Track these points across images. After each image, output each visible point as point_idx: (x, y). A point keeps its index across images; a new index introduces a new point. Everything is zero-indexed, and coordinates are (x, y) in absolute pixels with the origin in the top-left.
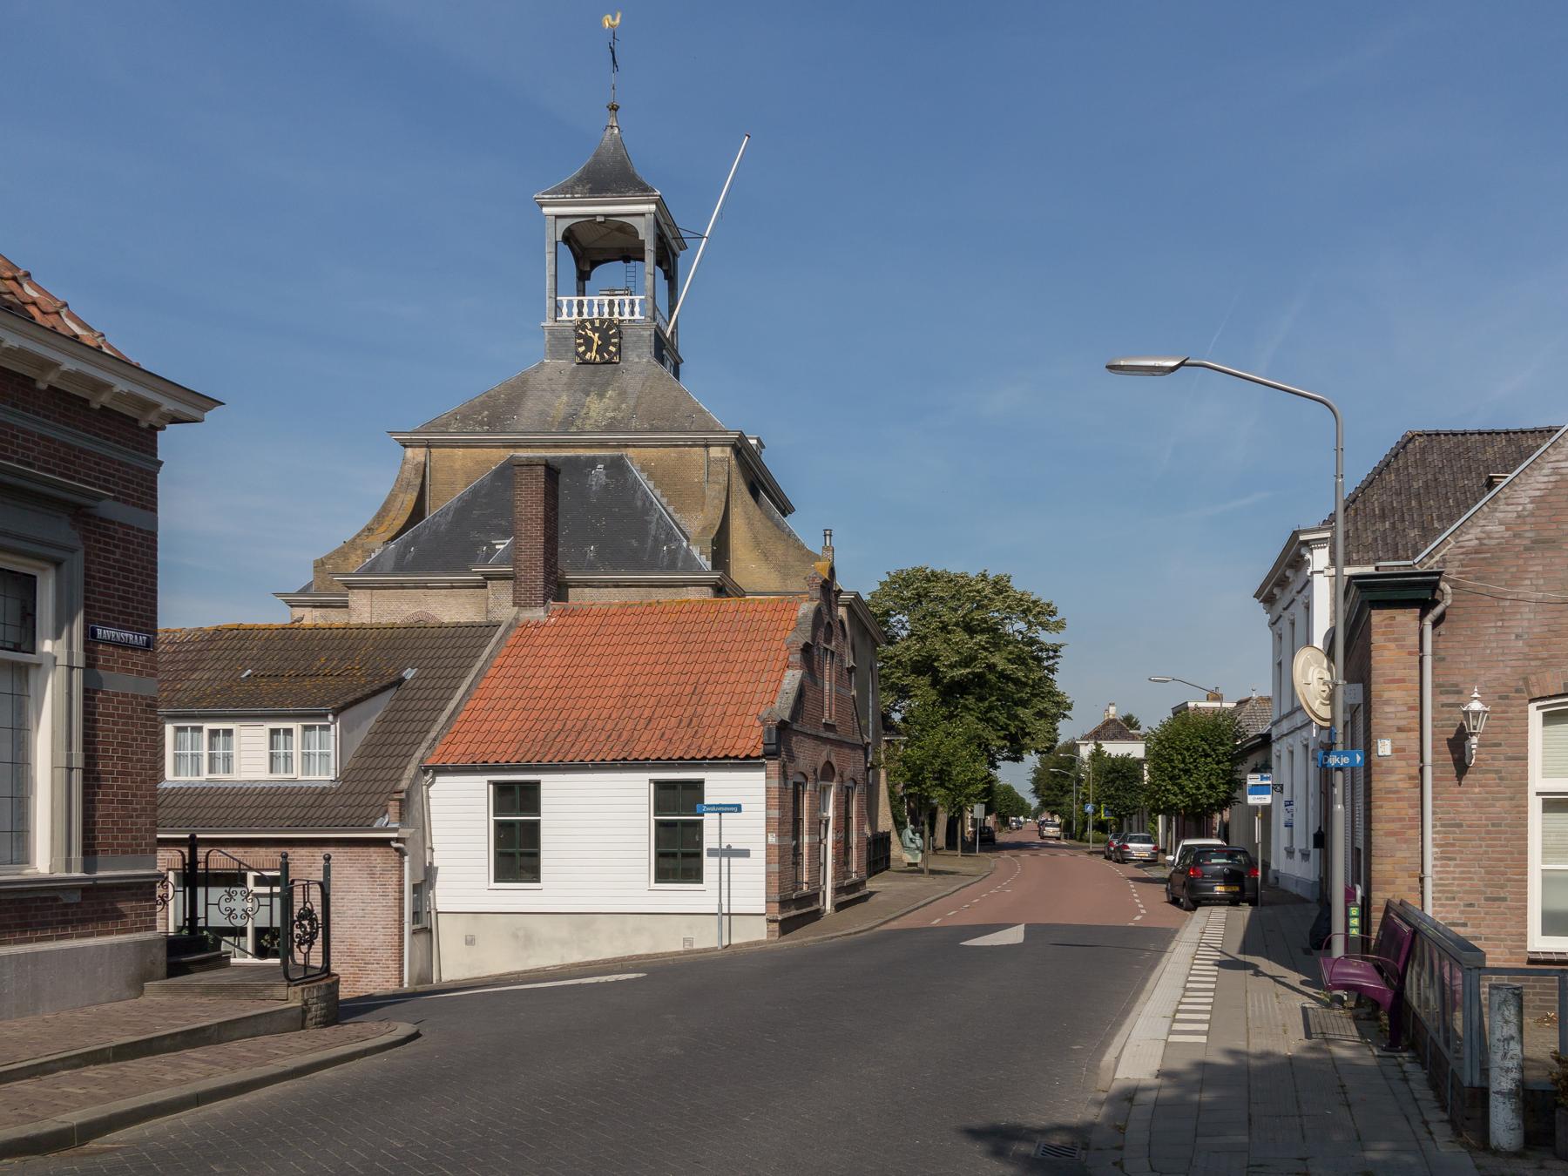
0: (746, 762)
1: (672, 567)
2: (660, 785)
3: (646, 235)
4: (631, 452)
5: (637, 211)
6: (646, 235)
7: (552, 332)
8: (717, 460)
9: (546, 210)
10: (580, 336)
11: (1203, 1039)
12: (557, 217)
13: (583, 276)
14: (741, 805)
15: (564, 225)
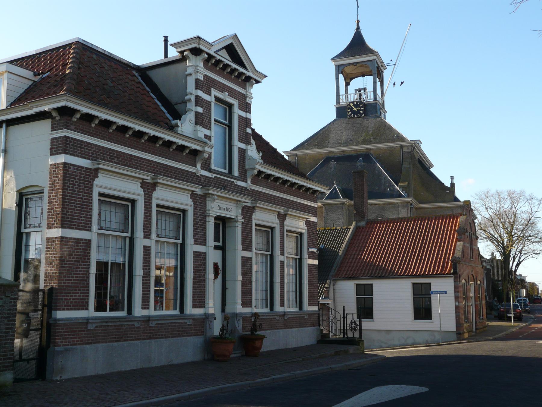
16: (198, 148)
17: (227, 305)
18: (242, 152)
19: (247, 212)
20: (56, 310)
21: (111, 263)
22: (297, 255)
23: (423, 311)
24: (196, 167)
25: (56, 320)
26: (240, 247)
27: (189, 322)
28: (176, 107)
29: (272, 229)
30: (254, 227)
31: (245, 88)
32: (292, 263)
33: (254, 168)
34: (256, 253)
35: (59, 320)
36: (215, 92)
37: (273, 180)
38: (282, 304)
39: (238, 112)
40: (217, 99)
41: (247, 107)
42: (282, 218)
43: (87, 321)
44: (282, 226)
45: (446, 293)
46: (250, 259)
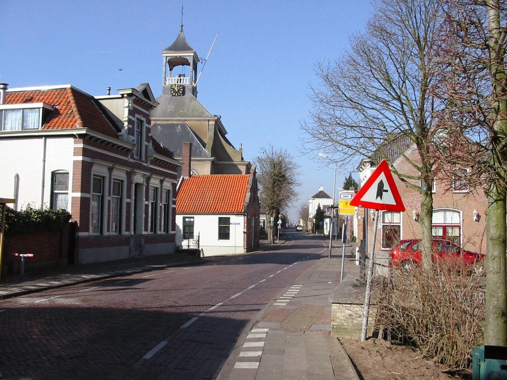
0: (238, 214)
1: (201, 156)
2: (220, 218)
3: (191, 61)
4: (187, 122)
5: (188, 55)
6: (191, 61)
7: (164, 87)
8: (211, 125)
9: (164, 55)
10: (172, 89)
11: (255, 365)
12: (167, 57)
13: (171, 69)
14: (238, 225)
15: (168, 59)
16: (130, 148)
17: (137, 230)
18: (146, 146)
19: (148, 179)
20: (78, 232)
21: (229, 218)
22: (154, 200)
23: (224, 234)
24: (128, 157)
25: (78, 236)
26: (144, 199)
27: (123, 239)
28: (116, 123)
29: (104, 178)
30: (92, 177)
31: (148, 111)
32: (115, 201)
33: (153, 156)
34: (93, 195)
35: (80, 236)
36: (137, 116)
37: (106, 144)
38: (108, 231)
39: (145, 125)
40: (137, 119)
41: (149, 122)
42: (110, 170)
43: (89, 237)
44: (161, 186)
45: (240, 224)
46: (89, 199)
